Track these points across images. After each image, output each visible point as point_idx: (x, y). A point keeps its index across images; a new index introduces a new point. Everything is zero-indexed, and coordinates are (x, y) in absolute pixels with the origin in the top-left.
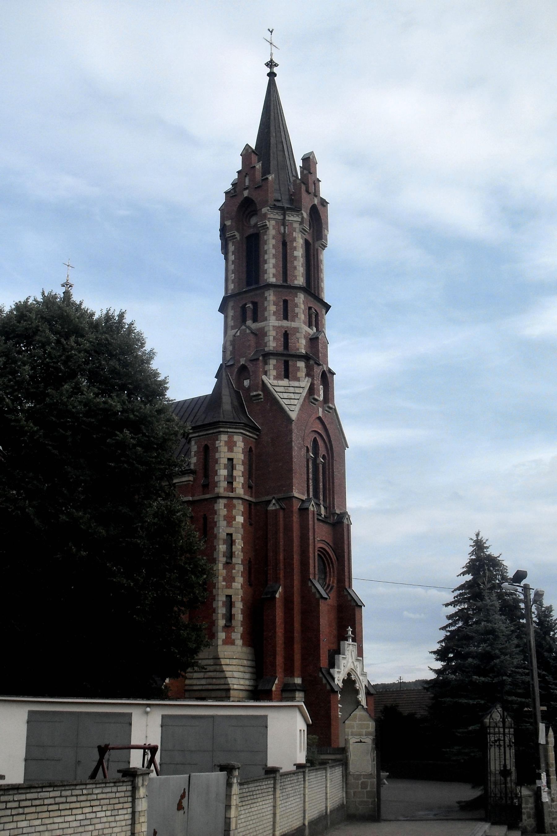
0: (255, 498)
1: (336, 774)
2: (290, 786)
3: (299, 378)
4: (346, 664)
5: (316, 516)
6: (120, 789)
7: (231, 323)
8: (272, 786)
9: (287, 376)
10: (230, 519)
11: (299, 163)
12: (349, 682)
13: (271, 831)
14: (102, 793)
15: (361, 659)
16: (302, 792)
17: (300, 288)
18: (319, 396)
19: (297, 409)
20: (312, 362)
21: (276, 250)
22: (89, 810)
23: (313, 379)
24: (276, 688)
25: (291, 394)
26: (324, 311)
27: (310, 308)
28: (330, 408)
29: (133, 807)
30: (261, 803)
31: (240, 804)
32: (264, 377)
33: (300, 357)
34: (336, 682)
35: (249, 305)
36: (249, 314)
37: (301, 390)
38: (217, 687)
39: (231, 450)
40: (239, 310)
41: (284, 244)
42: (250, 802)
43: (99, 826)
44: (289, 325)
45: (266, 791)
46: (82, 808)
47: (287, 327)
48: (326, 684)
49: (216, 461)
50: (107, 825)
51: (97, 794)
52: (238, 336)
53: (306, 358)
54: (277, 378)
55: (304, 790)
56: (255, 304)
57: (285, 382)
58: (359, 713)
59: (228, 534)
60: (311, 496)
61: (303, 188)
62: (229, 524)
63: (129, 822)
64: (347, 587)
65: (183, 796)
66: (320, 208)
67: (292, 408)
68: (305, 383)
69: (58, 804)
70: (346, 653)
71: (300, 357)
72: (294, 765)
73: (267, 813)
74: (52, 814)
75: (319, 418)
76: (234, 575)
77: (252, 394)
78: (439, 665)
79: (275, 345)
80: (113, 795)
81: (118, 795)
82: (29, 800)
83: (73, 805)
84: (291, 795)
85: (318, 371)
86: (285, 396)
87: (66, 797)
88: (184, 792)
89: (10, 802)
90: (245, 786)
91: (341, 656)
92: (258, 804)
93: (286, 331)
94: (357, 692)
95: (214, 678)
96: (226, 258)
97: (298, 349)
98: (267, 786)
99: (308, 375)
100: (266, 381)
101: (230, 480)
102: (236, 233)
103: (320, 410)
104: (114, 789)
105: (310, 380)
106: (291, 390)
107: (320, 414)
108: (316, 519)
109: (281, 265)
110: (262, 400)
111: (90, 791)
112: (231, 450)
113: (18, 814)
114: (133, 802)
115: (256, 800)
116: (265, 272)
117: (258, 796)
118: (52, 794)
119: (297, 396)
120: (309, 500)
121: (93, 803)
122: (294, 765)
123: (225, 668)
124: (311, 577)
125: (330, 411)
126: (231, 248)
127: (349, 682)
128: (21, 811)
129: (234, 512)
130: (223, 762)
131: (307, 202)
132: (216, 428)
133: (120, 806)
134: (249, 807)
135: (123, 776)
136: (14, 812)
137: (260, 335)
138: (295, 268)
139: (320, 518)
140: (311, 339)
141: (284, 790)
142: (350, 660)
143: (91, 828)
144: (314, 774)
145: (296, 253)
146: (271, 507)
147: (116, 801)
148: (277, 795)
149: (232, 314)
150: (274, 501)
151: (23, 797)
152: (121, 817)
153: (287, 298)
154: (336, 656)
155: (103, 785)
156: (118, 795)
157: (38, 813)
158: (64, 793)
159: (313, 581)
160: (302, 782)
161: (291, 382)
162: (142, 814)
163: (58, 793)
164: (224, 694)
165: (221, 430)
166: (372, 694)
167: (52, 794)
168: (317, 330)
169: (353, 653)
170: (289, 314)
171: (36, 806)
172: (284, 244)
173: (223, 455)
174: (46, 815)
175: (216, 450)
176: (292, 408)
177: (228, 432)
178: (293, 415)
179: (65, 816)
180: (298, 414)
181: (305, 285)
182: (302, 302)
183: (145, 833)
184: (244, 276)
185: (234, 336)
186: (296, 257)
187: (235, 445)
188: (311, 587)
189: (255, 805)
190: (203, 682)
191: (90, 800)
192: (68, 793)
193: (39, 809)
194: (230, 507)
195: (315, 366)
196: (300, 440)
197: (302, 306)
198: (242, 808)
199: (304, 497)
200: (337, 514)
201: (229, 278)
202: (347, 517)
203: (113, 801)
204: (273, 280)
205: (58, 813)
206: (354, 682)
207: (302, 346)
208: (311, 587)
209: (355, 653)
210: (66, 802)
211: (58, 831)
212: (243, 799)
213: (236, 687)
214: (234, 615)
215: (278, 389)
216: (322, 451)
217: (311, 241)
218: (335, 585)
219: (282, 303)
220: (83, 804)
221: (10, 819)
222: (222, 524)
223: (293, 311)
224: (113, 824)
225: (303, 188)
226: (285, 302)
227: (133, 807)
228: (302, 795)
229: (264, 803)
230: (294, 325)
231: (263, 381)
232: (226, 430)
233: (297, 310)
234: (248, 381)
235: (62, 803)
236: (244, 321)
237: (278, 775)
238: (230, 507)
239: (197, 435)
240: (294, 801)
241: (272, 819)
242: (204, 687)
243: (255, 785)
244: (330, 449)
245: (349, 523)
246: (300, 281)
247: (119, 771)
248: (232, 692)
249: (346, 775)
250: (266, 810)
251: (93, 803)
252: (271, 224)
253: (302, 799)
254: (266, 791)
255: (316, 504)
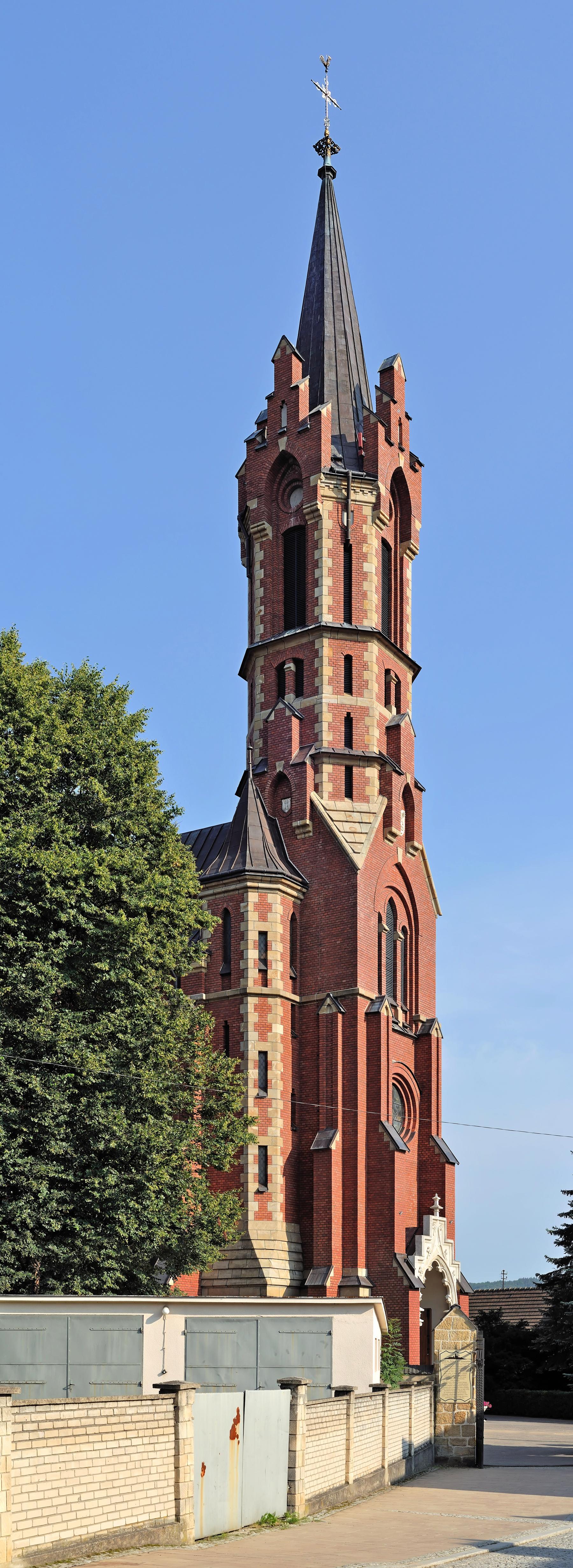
0: (300, 995)
1: (422, 1398)
2: (367, 1413)
3: (368, 796)
4: (434, 1247)
5: (391, 1024)
6: (159, 1409)
7: (260, 698)
8: (345, 1412)
9: (349, 794)
10: (264, 1029)
11: (375, 380)
12: (435, 1275)
13: (344, 1472)
14: (138, 1414)
15: (452, 1241)
16: (381, 1423)
17: (370, 634)
18: (399, 828)
19: (364, 850)
20: (388, 769)
21: (333, 559)
22: (123, 1435)
23: (390, 799)
24: (332, 1283)
25: (354, 820)
26: (410, 675)
27: (387, 672)
28: (416, 849)
29: (176, 1433)
30: (331, 1435)
31: (307, 1434)
32: (313, 795)
33: (368, 760)
34: (417, 1274)
35: (291, 666)
36: (290, 681)
37: (371, 818)
38: (248, 1282)
39: (263, 918)
40: (273, 673)
41: (348, 549)
42: (319, 1431)
43: (135, 1457)
44: (354, 703)
45: (337, 1418)
46: (114, 1432)
47: (351, 706)
48: (402, 1278)
49: (243, 936)
50: (145, 1456)
51: (131, 1415)
52: (272, 721)
53: (379, 760)
54: (333, 796)
55: (384, 1421)
56: (298, 662)
57: (346, 804)
58: (452, 1315)
59: (260, 1052)
60: (384, 993)
61: (381, 430)
62: (263, 1038)
63: (172, 1452)
64: (434, 1134)
65: (237, 1421)
66: (408, 474)
67: (357, 847)
68: (378, 804)
69: (85, 1426)
70: (431, 1231)
71: (368, 760)
72: (370, 1386)
73: (339, 1448)
74: (78, 1440)
75: (399, 866)
76: (269, 1115)
77: (294, 824)
78: (561, 1253)
79: (331, 738)
80: (150, 1417)
81: (157, 1417)
82: (50, 1421)
83: (103, 1429)
84: (367, 1426)
85: (398, 784)
86: (347, 827)
87: (94, 1418)
88: (238, 1416)
89: (27, 1422)
90: (313, 1410)
91: (424, 1237)
92: (328, 1435)
93: (348, 714)
94: (446, 1290)
95: (242, 1269)
96: (250, 575)
97: (367, 746)
98: (339, 1412)
99: (382, 792)
100: (317, 802)
101: (263, 968)
102: (267, 525)
103: (401, 851)
104: (152, 1409)
105: (386, 800)
106: (356, 817)
107: (400, 860)
108: (390, 1029)
109: (281, 587)
110: (311, 834)
111: (123, 1411)
112: (263, 918)
113: (39, 1439)
114: (176, 1426)
115: (326, 1430)
116: (316, 602)
117: (328, 1424)
118: (77, 1414)
119: (365, 828)
120: (381, 999)
121: (127, 1427)
122: (370, 1386)
123: (258, 1254)
124: (383, 1119)
125: (415, 853)
126: (259, 555)
127: (435, 1275)
128: (41, 1434)
129: (270, 1017)
130: (286, 1376)
131: (389, 461)
132: (240, 881)
133: (160, 1431)
134: (317, 1438)
135: (160, 1392)
136: (33, 1436)
137: (310, 719)
138: (365, 595)
139: (396, 1028)
140: (388, 728)
141: (359, 1419)
142: (437, 1244)
143: (125, 1459)
144: (395, 1399)
145: (366, 567)
146: (324, 1011)
147: (155, 1424)
148: (352, 1425)
149: (261, 681)
150: (328, 1001)
151: (42, 1417)
152: (162, 1447)
153: (350, 653)
154: (417, 1237)
155: (139, 1403)
156: (157, 1417)
157: (62, 1437)
158: (92, 1413)
159: (386, 1124)
160: (381, 1410)
161: (355, 804)
162: (187, 1442)
163: (83, 1413)
164: (258, 1290)
165: (249, 884)
166: (466, 1294)
167: (77, 1414)
168: (398, 712)
169: (440, 1232)
170: (354, 683)
171: (58, 1429)
172: (348, 549)
173: (253, 926)
174: (70, 1440)
175: (242, 917)
176: (357, 847)
177: (258, 888)
178: (359, 861)
179: (93, 1442)
180: (366, 859)
181: (380, 629)
182: (375, 660)
183: (192, 1467)
184: (280, 609)
185: (266, 721)
186: (366, 573)
187: (270, 910)
188: (382, 1134)
189: (324, 1436)
190: (228, 1274)
191: (123, 1423)
192: (96, 1413)
193: (63, 1433)
194: (263, 1010)
195: (394, 775)
196: (369, 903)
197: (375, 668)
198: (309, 1439)
199: (374, 996)
200: (423, 1022)
201: (256, 613)
202: (436, 1026)
203: (150, 1425)
204: (327, 619)
205: (85, 1439)
206: (442, 1275)
207: (373, 741)
208: (382, 1134)
209: (443, 1233)
210: (95, 1425)
211: (87, 1461)
212: (310, 1427)
213: (274, 1281)
214: (271, 1175)
215: (334, 815)
216: (402, 921)
217: (392, 543)
218: (416, 1131)
219: (342, 663)
220: (115, 1428)
221: (28, 1445)
222: (252, 1036)
223: (360, 676)
224: (152, 1455)
225: (381, 430)
226: (348, 659)
227: (176, 1433)
228: (381, 1427)
229: (335, 1434)
230: (361, 702)
231: (312, 802)
232: (256, 885)
233: (366, 675)
234: (289, 800)
235: (90, 1426)
236: (281, 694)
237: (353, 1395)
238: (263, 1010)
239: (210, 892)
240: (370, 1435)
241: (344, 1457)
242: (229, 1283)
243: (325, 1409)
244: (414, 917)
245: (440, 1036)
246: (372, 620)
247: (155, 1386)
248: (268, 1288)
249: (435, 1401)
250: (337, 1444)
251: (127, 1427)
252: (326, 507)
253: (381, 1432)
254: (337, 1418)
255: (392, 1005)
